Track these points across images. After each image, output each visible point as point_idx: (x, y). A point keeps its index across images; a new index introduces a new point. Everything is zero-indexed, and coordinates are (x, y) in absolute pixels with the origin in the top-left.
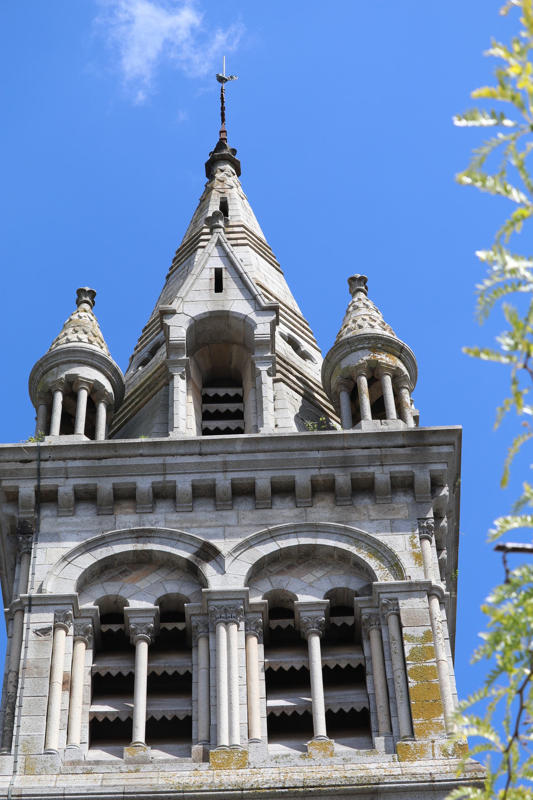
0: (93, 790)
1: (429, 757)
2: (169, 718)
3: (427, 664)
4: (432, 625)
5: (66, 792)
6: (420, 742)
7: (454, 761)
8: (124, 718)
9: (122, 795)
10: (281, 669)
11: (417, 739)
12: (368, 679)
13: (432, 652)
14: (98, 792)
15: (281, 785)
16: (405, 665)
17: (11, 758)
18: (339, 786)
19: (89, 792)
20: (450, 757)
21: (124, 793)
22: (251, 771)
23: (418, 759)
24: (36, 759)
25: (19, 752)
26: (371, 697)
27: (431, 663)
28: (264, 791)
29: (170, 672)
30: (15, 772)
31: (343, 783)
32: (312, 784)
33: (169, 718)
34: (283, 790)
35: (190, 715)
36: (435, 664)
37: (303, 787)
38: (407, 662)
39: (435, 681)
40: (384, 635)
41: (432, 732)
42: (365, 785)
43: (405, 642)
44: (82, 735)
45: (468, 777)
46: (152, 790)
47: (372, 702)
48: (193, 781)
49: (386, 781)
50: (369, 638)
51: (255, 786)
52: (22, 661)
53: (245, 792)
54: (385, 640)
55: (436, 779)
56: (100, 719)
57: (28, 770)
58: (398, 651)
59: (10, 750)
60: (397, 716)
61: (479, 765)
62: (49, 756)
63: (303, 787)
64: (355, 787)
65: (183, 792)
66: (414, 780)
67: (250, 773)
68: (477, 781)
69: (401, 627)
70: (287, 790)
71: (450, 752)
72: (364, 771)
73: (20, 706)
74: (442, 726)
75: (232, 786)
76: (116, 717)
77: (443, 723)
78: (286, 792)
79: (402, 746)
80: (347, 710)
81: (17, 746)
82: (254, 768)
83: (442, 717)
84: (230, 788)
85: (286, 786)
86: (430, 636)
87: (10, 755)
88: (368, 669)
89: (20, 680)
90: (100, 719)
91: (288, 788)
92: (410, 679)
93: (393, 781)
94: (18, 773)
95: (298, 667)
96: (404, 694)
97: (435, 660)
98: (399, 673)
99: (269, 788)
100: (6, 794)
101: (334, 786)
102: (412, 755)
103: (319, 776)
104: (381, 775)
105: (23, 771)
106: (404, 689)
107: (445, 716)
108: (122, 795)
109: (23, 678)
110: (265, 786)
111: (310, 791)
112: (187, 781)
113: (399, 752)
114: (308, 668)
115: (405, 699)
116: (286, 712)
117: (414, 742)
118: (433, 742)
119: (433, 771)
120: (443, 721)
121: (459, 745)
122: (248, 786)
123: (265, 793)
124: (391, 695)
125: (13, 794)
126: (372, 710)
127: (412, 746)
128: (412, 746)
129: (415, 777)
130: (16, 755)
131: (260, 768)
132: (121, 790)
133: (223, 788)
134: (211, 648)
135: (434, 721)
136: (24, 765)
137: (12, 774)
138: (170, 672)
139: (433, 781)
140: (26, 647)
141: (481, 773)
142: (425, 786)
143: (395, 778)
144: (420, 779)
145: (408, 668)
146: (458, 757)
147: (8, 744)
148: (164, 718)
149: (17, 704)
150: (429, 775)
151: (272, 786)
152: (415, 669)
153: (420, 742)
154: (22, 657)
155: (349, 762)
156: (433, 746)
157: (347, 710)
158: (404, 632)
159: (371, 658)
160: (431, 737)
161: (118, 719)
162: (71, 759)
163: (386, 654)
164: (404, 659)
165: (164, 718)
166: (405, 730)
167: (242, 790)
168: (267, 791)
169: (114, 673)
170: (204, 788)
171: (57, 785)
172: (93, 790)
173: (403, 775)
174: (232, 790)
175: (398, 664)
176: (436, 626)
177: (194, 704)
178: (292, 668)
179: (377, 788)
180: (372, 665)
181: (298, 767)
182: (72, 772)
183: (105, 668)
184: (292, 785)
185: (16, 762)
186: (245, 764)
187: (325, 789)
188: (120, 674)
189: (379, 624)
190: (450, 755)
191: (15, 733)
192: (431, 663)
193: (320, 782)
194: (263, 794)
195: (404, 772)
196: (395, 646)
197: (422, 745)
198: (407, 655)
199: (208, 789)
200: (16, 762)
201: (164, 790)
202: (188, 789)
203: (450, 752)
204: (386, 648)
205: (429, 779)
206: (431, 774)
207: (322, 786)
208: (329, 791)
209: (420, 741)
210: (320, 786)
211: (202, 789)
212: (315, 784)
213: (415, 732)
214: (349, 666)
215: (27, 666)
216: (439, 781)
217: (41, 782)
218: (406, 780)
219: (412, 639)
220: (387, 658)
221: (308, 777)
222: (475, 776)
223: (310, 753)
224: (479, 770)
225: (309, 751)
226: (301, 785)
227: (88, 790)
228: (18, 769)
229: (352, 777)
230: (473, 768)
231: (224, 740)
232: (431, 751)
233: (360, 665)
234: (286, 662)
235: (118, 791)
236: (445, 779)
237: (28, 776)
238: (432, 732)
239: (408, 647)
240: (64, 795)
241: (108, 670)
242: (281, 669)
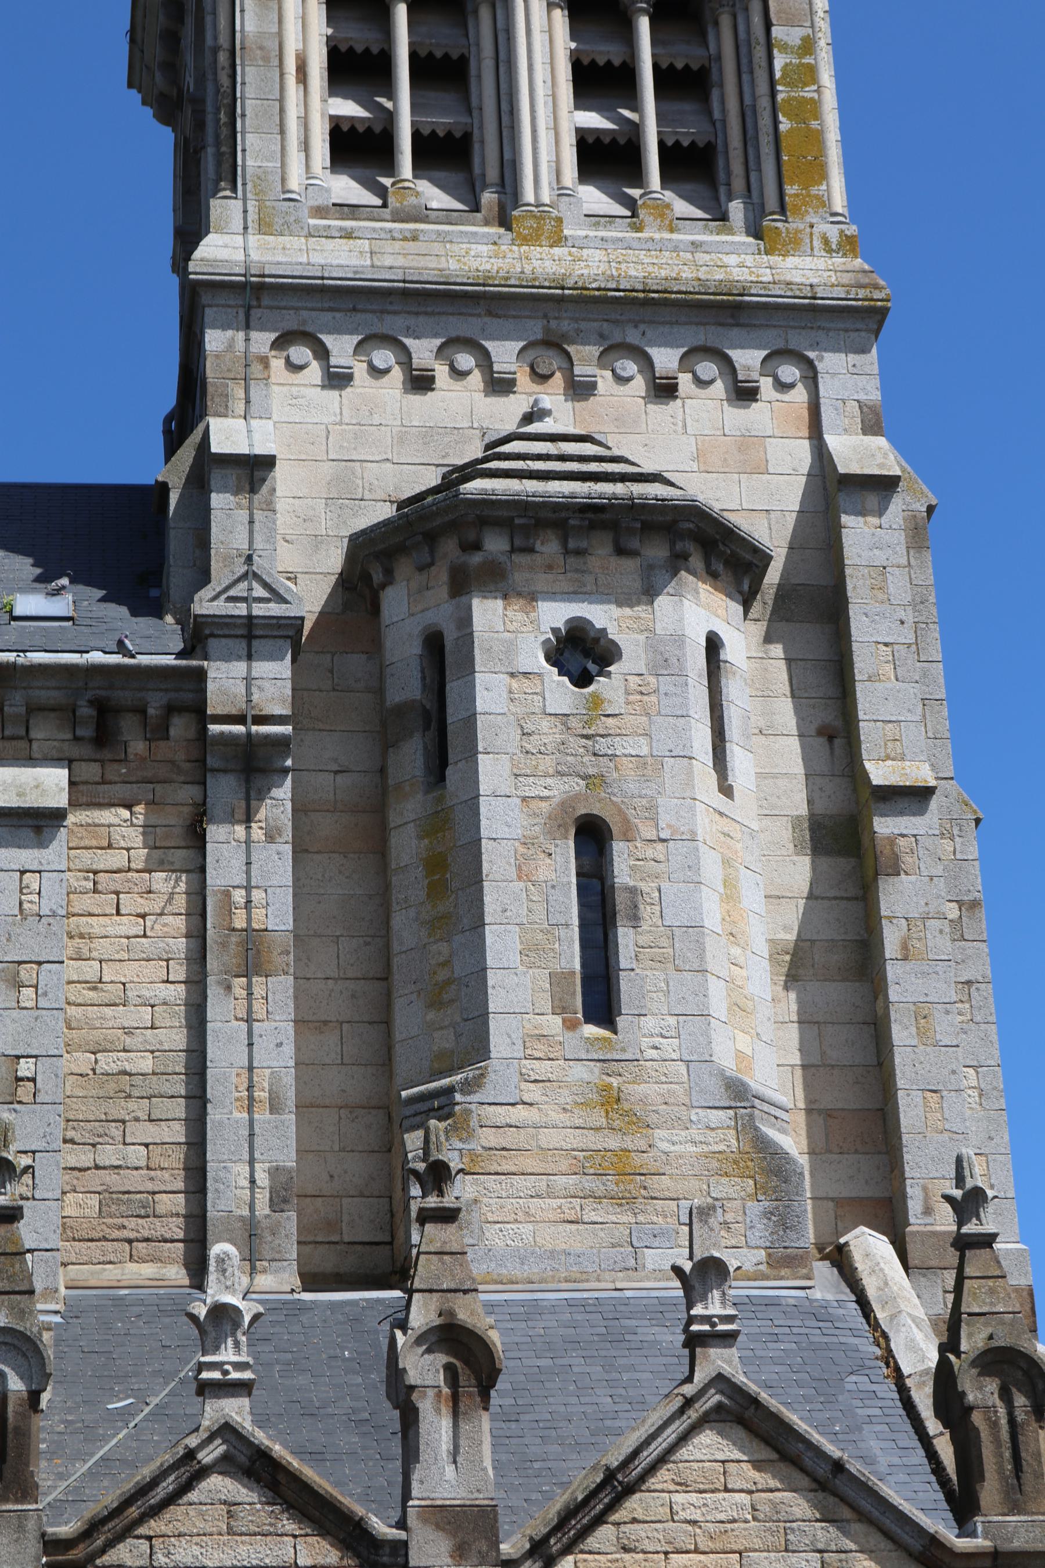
0: (363, 273)
1: (805, 251)
2: (441, 134)
3: (806, 94)
4: (812, 26)
5: (326, 275)
6: (794, 225)
7: (838, 261)
8: (378, 129)
9: (401, 285)
10: (593, 62)
11: (790, 220)
12: (715, 94)
13: (810, 74)
14: (369, 277)
15: (614, 286)
16: (773, 94)
17: (236, 205)
18: (691, 293)
19: (357, 276)
20: (834, 255)
21: (404, 281)
22: (570, 254)
23: (792, 252)
24: (274, 208)
25: (249, 195)
26: (718, 125)
27: (809, 93)
28: (592, 293)
29: (439, 54)
30: (246, 228)
31: (697, 290)
32: (655, 288)
33: (441, 134)
34: (617, 294)
35: (470, 130)
36: (815, 95)
37: (643, 291)
38: (779, 88)
39: (814, 124)
40: (741, 28)
41: (810, 210)
42: (724, 295)
43: (775, 52)
44: (324, 160)
45: (860, 296)
46: (442, 280)
47: (720, 134)
48: (495, 268)
49: (753, 291)
50: (716, 24)
51: (580, 284)
52: (238, 35)
53: (567, 292)
54: (742, 35)
55: (819, 295)
56: (345, 128)
57: (265, 227)
58: (764, 64)
59: (234, 189)
60: (759, 170)
61: (874, 275)
62: (292, 204)
63: (643, 291)
64: (712, 297)
65: (484, 285)
66: (789, 293)
67: (570, 258)
68: (872, 303)
69: (768, 25)
70: (622, 294)
71: (834, 247)
72: (723, 270)
73: (243, 115)
74: (824, 202)
75: (550, 280)
76: (367, 125)
77: (825, 198)
78: (621, 297)
79: (770, 229)
80: (686, 143)
81: (244, 184)
82: (573, 247)
83: (824, 187)
84: (547, 284)
85: (622, 287)
86: (808, 46)
87: (236, 198)
88: (715, 76)
89: (239, 69)
90: (345, 128)
91: (624, 291)
92: (781, 118)
93: (762, 292)
94: (250, 230)
95: (617, 62)
96: (771, 138)
97: (815, 87)
98: (764, 102)
99: (598, 289)
100: (243, 272)
101: (685, 293)
102: (784, 246)
103: (663, 273)
104: (746, 281)
105: (257, 227)
106: (771, 130)
107: (828, 186)
108: (401, 285)
109: (243, 65)
110: (594, 285)
111: (653, 298)
112: (488, 267)
113: (766, 239)
114: (631, 66)
115: (772, 147)
116: (602, 137)
117: (786, 225)
118: (812, 226)
119: (815, 281)
120: (826, 194)
121: (846, 235)
122: (570, 283)
123: (594, 297)
124: (750, 133)
125: (253, 272)
126: (720, 147)
127: (784, 230)
128: (784, 230)
129: (792, 290)
130: (245, 200)
131: (582, 248)
132: (400, 277)
133: (537, 284)
134: (500, 25)
135: (814, 190)
136: (257, 217)
137: (242, 231)
138: (439, 54)
139: (815, 298)
140: (242, 11)
141: (877, 291)
142: (803, 305)
143: (765, 288)
144: (798, 293)
145: (780, 97)
146: (845, 255)
147: (230, 177)
148: (433, 133)
149: (239, 110)
150: (809, 288)
151: (603, 286)
152: (787, 101)
153: (794, 225)
154: (238, 27)
155: (699, 249)
156: (811, 234)
157: (686, 143)
158: (774, 35)
159: (719, 58)
160: (809, 219)
161: (369, 130)
162: (316, 203)
163: (744, 61)
164: (772, 83)
165: (433, 133)
166: (772, 203)
167: (563, 288)
168: (597, 293)
169: (359, 48)
170: (512, 282)
171: (312, 261)
172: (363, 273)
173: (775, 283)
174: (550, 288)
175: (763, 88)
176: (817, 25)
177: (475, 113)
178: (609, 63)
179: (742, 302)
180: (721, 70)
181: (631, 252)
182: (325, 234)
183: (347, 39)
184: (628, 287)
185: (245, 211)
186: (560, 240)
187: (673, 296)
188: (367, 50)
189: (734, 5)
190: (834, 251)
191: (239, 162)
192: (809, 93)
193: (666, 285)
194: (590, 297)
195: (777, 278)
196: (760, 53)
197: (797, 231)
198: (778, 75)
199: (517, 283)
200: (245, 211)
201: (459, 280)
202: (490, 282)
203: (834, 247)
204: (743, 50)
205: (809, 295)
206: (811, 286)
207: (669, 292)
208: (677, 300)
209: (795, 224)
210: (665, 291)
211: (509, 283)
212: (660, 288)
213: (789, 207)
214: (687, 67)
215: (247, 45)
216: (823, 299)
217: (287, 252)
218: (779, 293)
219: (785, 48)
220: (744, 68)
221: (650, 273)
222: (869, 295)
223: (642, 221)
224: (876, 287)
225: (641, 216)
226: (640, 287)
227: (355, 272)
228: (250, 224)
229: (707, 280)
230: (867, 281)
231: (529, 196)
232: (808, 241)
233: (703, 67)
234: (601, 53)
235: (396, 278)
236: (830, 296)
237: (266, 237)
238: (810, 210)
239: (779, 63)
240: (323, 278)
241: (351, 43)
242: (593, 62)
